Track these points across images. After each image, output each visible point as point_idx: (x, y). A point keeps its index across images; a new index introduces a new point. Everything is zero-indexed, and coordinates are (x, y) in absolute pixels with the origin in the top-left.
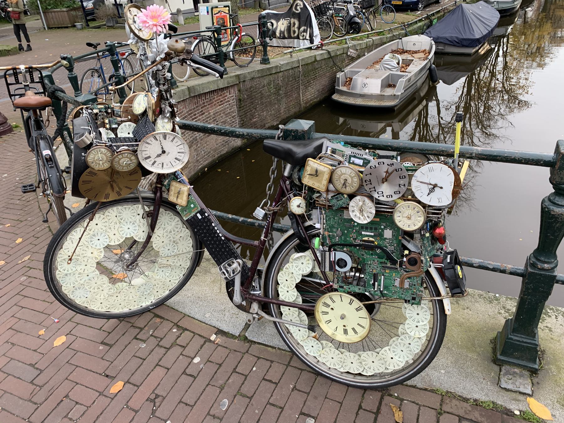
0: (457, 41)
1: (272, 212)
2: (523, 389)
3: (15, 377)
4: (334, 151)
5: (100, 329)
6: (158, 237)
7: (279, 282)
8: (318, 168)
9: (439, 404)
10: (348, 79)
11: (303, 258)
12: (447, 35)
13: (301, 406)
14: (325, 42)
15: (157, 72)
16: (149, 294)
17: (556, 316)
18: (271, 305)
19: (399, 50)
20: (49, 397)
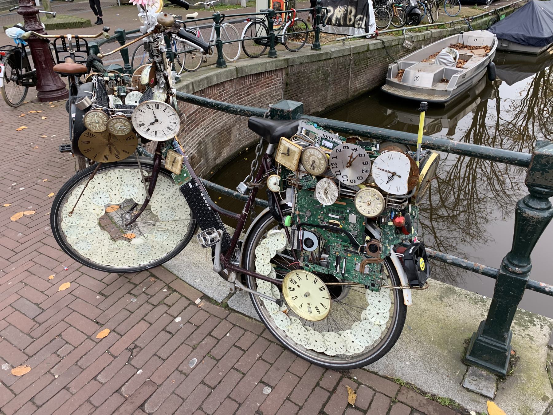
0: (523, 39)
1: (253, 187)
2: (486, 392)
3: (21, 312)
4: (307, 133)
5: (100, 281)
6: (156, 202)
7: (257, 255)
8: (290, 147)
9: (395, 393)
10: (401, 71)
11: (279, 235)
12: (513, 33)
13: (262, 375)
14: (381, 32)
15: (150, 44)
16: (147, 254)
17: (542, 326)
18: (248, 276)
19: (458, 45)
20: (45, 333)
